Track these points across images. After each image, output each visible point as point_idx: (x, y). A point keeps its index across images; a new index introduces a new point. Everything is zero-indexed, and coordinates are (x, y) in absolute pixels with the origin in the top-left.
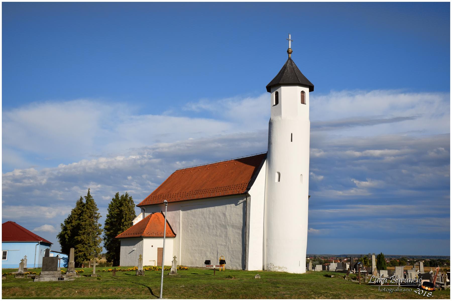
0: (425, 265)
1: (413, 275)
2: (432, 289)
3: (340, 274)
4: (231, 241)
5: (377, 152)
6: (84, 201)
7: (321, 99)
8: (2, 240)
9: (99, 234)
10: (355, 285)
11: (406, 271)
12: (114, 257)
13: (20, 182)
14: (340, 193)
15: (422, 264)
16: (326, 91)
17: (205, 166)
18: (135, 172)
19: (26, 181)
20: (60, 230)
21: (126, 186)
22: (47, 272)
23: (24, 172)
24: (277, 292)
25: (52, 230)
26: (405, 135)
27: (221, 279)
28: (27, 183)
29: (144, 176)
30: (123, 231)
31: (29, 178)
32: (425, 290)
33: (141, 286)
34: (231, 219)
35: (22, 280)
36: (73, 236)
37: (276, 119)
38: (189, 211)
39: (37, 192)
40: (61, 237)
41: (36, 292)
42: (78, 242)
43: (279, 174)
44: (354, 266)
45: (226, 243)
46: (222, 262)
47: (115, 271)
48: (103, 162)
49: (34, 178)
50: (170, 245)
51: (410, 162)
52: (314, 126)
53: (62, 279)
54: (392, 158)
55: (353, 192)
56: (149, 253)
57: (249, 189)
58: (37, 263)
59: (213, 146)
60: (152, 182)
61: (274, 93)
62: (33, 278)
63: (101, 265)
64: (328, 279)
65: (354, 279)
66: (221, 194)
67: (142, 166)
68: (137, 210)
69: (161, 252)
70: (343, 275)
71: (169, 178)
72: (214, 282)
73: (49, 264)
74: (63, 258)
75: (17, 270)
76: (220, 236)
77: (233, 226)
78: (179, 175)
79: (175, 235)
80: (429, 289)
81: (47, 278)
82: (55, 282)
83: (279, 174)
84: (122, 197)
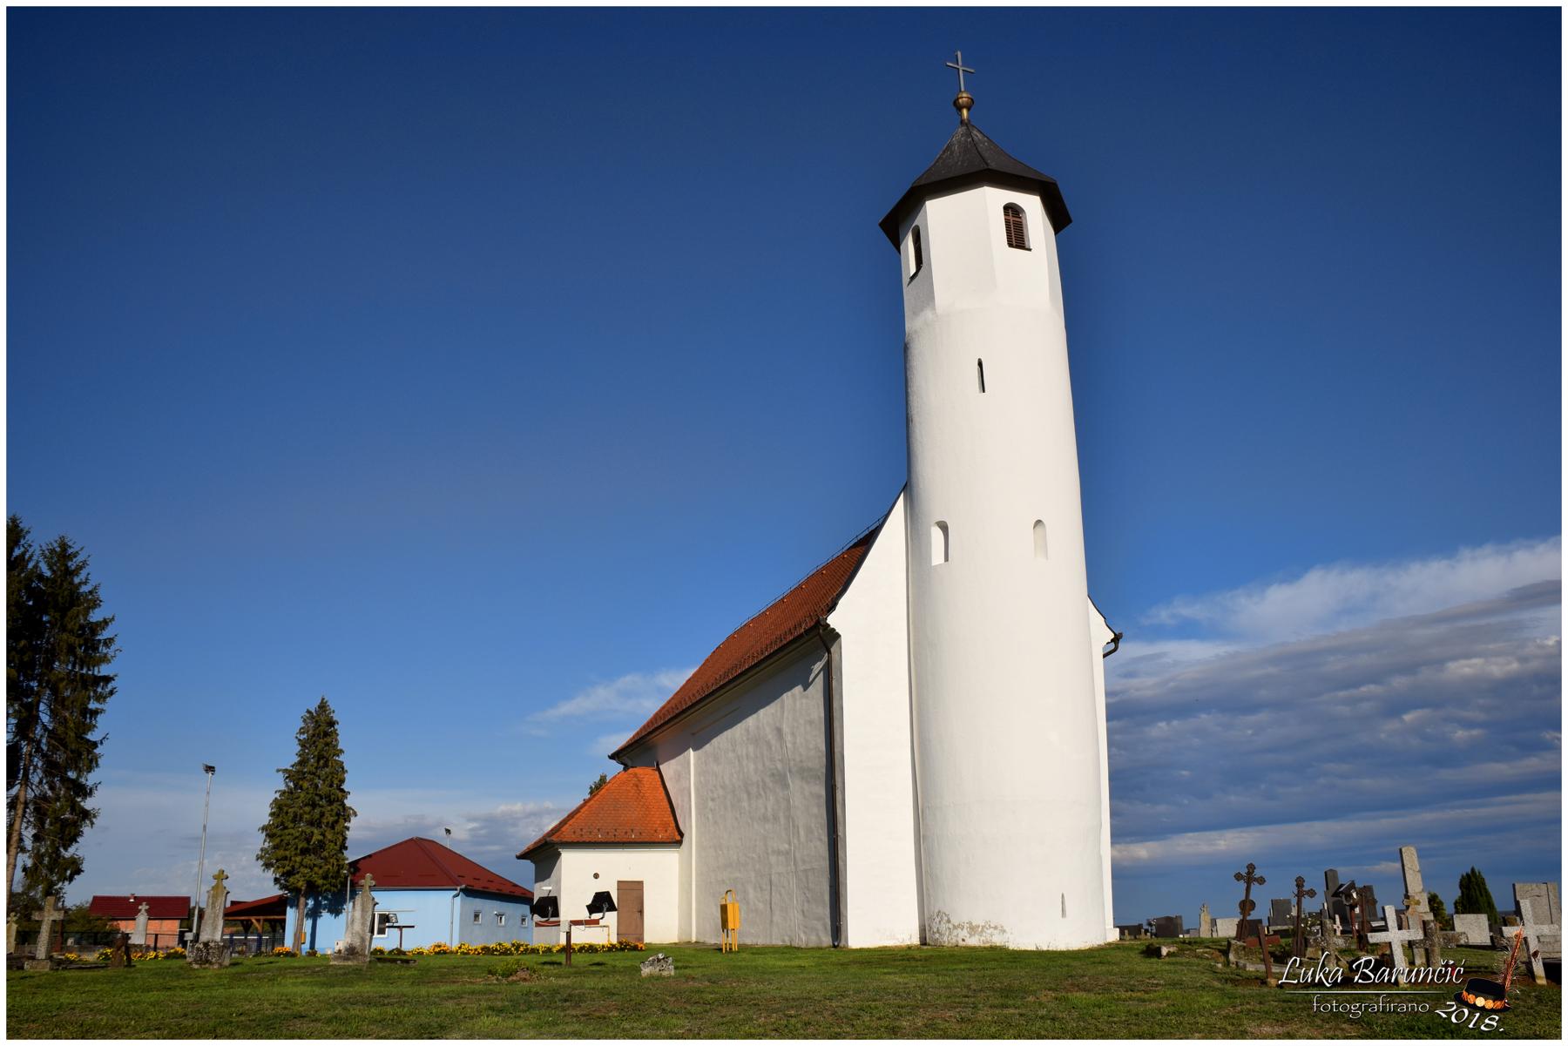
2: (1499, 1004)
4: (802, 833)
8: (1559, 966)
32: (1473, 1008)
43: (944, 527)
79: (681, 835)
80: (1490, 1004)
83: (944, 527)
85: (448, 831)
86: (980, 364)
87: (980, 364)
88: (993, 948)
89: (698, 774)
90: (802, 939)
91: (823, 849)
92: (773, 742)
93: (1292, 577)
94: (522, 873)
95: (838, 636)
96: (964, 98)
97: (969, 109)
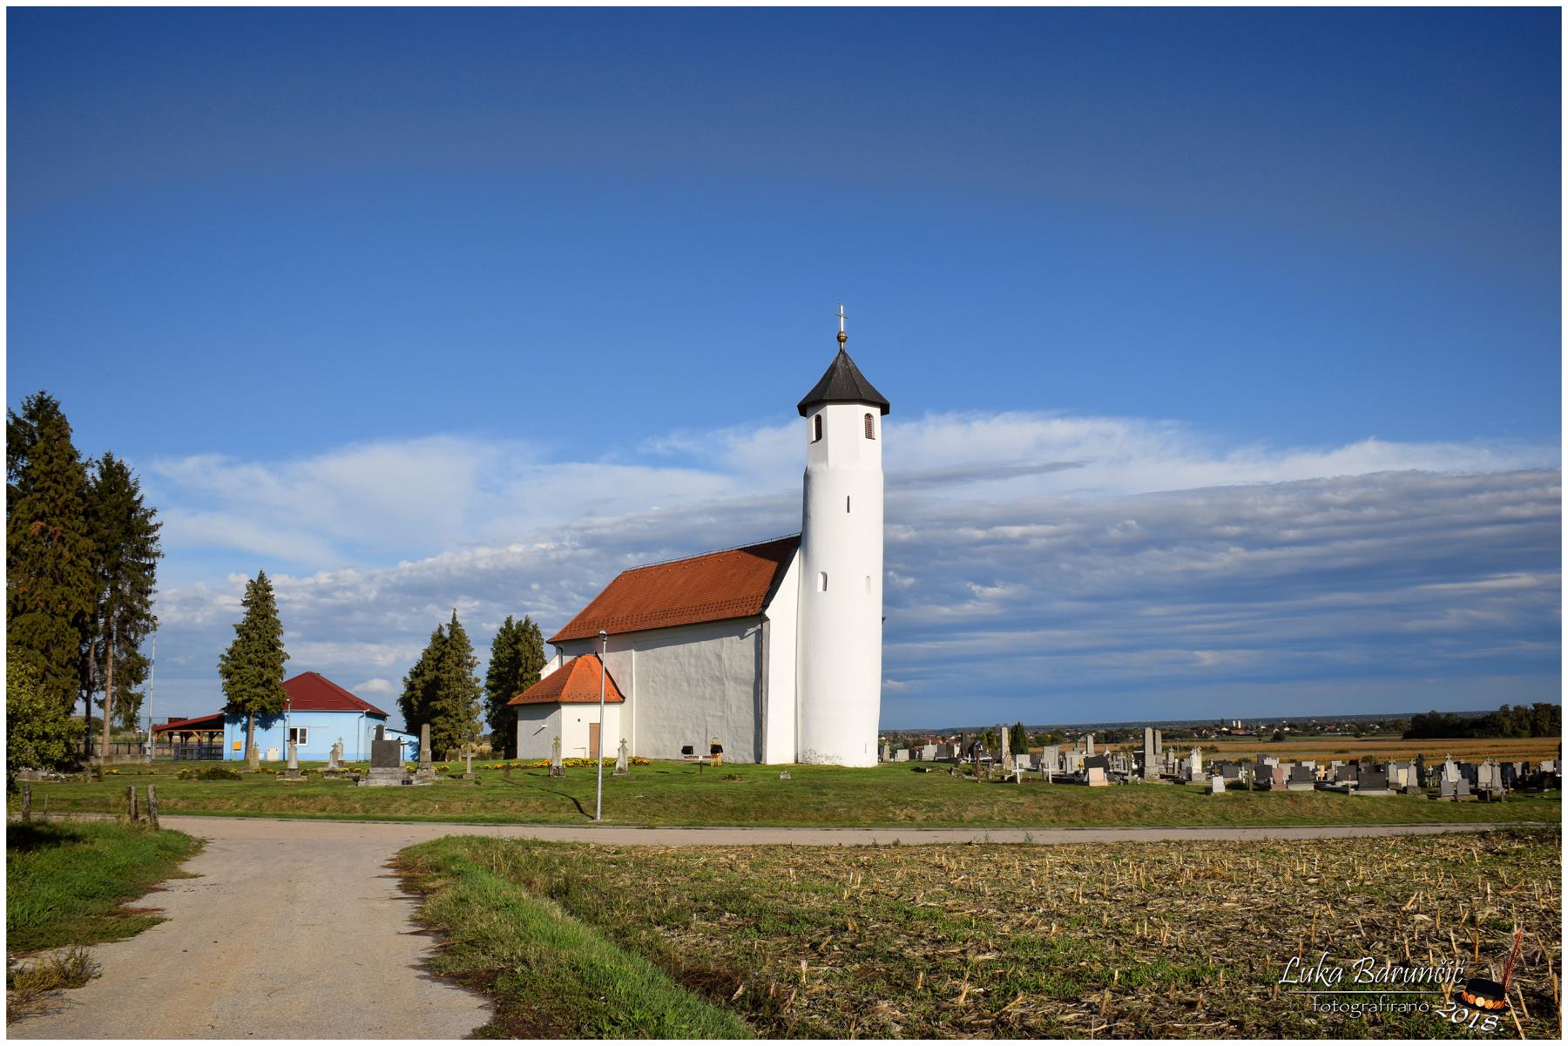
0: (1096, 742)
1: (1075, 761)
2: (1499, 1004)
3: (942, 765)
5: (1016, 531)
6: (446, 633)
7: (907, 429)
9: (477, 697)
10: (969, 786)
11: (1063, 754)
12: (505, 742)
13: (329, 596)
14: (946, 610)
15: (1090, 739)
16: (914, 414)
17: (680, 563)
18: (547, 575)
19: (338, 594)
20: (401, 690)
21: (528, 604)
22: (380, 770)
23: (336, 578)
24: (822, 803)
25: (387, 690)
26: (1067, 497)
27: (716, 781)
28: (342, 598)
29: (564, 583)
30: (521, 690)
31: (345, 589)
32: (1474, 1007)
33: (558, 798)
35: (337, 783)
36: (428, 699)
37: (817, 468)
38: (649, 652)
39: (360, 616)
40: (405, 702)
41: (363, 806)
42: (437, 713)
44: (970, 750)
46: (716, 749)
47: (508, 768)
48: (484, 557)
49: (353, 588)
50: (613, 719)
51: (1077, 550)
52: (893, 481)
53: (409, 782)
54: (1044, 541)
55: (969, 607)
56: (572, 733)
57: (765, 606)
58: (362, 752)
59: (700, 521)
60: (580, 594)
61: (813, 419)
62: (356, 780)
63: (482, 756)
64: (920, 776)
65: (969, 773)
66: (712, 616)
67: (559, 562)
68: (548, 650)
69: (596, 730)
70: (948, 766)
71: (610, 586)
72: (700, 787)
73: (384, 753)
74: (410, 744)
75: (326, 764)
77: (736, 679)
78: (630, 579)
80: (1490, 1004)
81: (381, 780)
82: (396, 788)
84: (519, 624)
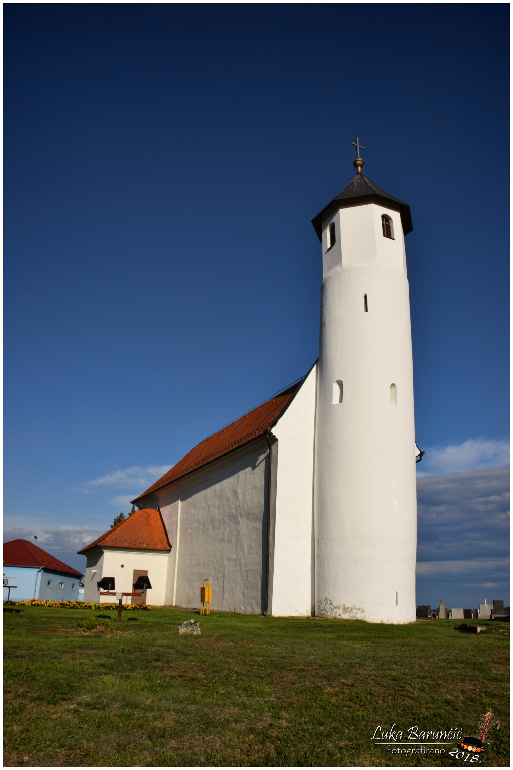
2: (479, 750)
32: (467, 751)
34: (244, 499)
43: (341, 384)
45: (237, 555)
50: (158, 567)
76: (229, 541)
79: (170, 546)
80: (475, 750)
83: (341, 384)
85: (36, 537)
86: (366, 297)
87: (366, 297)
88: (358, 621)
89: (182, 514)
90: (242, 609)
91: (259, 559)
92: (231, 498)
93: (458, 442)
94: (78, 563)
95: (276, 440)
96: (359, 161)
97: (361, 167)
